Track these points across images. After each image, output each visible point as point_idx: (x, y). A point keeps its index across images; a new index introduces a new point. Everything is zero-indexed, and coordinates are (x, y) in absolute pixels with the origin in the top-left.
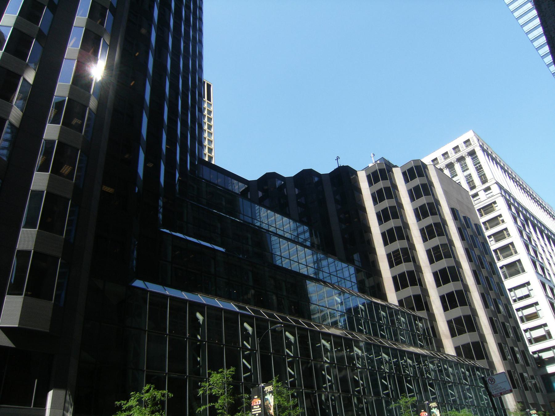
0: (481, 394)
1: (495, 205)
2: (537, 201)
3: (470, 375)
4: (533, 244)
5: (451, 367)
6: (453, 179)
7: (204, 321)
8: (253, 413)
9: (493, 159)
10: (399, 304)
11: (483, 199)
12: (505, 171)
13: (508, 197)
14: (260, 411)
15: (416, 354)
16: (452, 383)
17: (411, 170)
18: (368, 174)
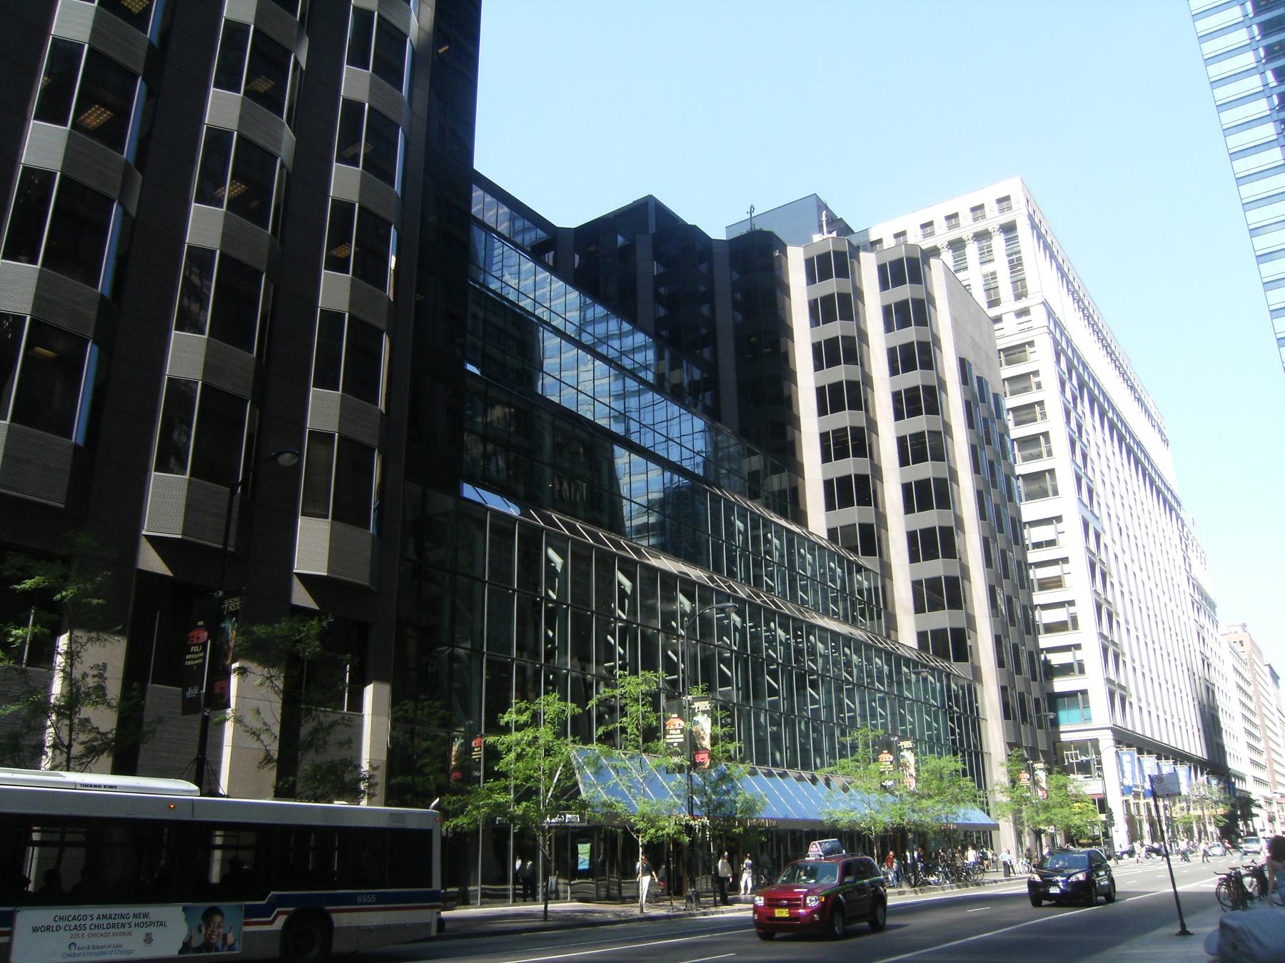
0: (873, 704)
1: (1032, 350)
2: (1088, 317)
3: (890, 671)
4: (1084, 440)
5: (824, 642)
6: (956, 275)
7: (565, 566)
8: (668, 741)
9: (1047, 247)
10: (829, 536)
11: (1009, 333)
12: (1063, 275)
13: (1058, 336)
14: (682, 740)
15: (833, 633)
16: (818, 675)
17: (897, 265)
18: (810, 256)
